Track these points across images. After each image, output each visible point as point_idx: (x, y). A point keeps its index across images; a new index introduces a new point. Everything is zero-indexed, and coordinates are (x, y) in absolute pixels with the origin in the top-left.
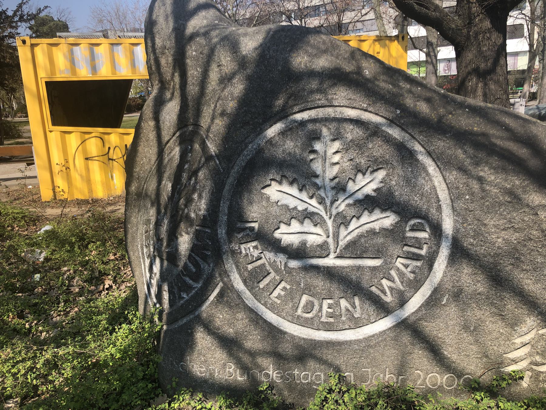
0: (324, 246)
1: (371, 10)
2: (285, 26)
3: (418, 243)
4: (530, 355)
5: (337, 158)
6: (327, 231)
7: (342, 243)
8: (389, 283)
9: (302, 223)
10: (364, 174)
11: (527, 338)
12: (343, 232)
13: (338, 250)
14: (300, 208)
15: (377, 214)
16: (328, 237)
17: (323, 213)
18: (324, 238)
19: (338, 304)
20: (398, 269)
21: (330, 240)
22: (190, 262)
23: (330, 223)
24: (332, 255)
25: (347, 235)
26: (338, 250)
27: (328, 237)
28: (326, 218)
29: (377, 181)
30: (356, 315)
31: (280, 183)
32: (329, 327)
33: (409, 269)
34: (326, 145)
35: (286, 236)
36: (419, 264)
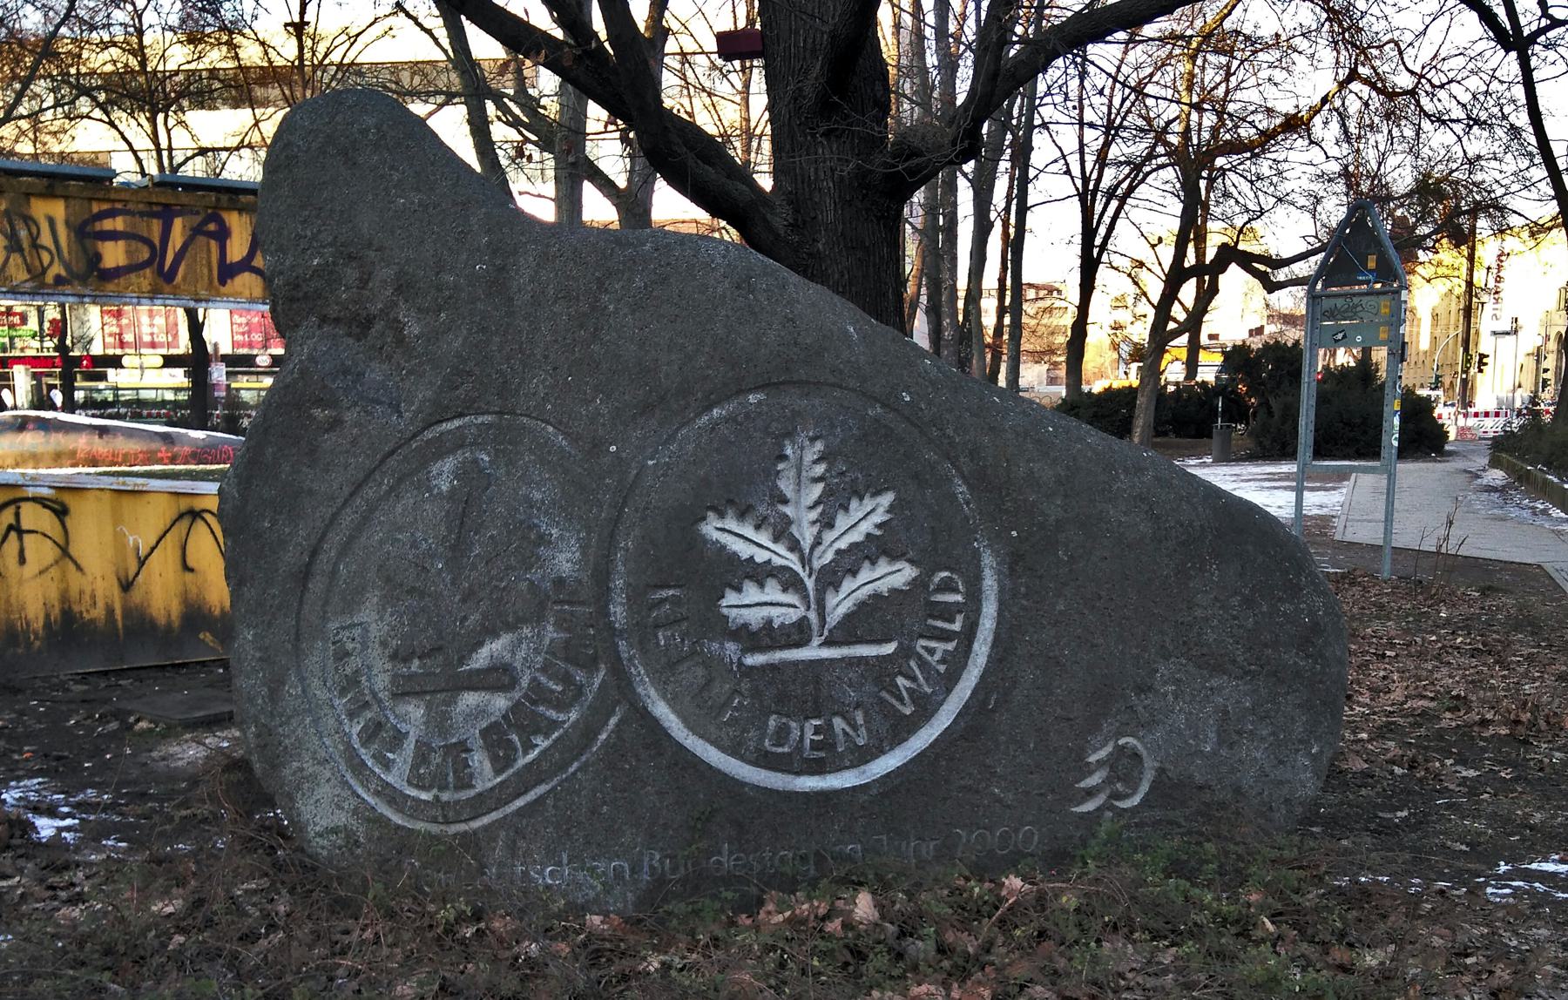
0: (802, 626)
1: (1148, 95)
2: (1189, 457)
3: (947, 613)
4: (1108, 781)
5: (820, 469)
6: (805, 597)
7: (834, 618)
8: (908, 684)
9: (762, 585)
10: (861, 499)
11: (1102, 754)
12: (831, 600)
13: (826, 633)
14: (758, 560)
15: (883, 567)
16: (809, 608)
17: (798, 568)
18: (801, 611)
19: (830, 725)
20: (920, 657)
21: (813, 616)
22: (516, 750)
23: (810, 584)
24: (816, 641)
25: (840, 604)
26: (826, 633)
27: (809, 608)
28: (803, 574)
29: (881, 510)
30: (861, 742)
31: (722, 515)
32: (818, 768)
33: (937, 657)
34: (802, 448)
35: (735, 610)
36: (950, 646)
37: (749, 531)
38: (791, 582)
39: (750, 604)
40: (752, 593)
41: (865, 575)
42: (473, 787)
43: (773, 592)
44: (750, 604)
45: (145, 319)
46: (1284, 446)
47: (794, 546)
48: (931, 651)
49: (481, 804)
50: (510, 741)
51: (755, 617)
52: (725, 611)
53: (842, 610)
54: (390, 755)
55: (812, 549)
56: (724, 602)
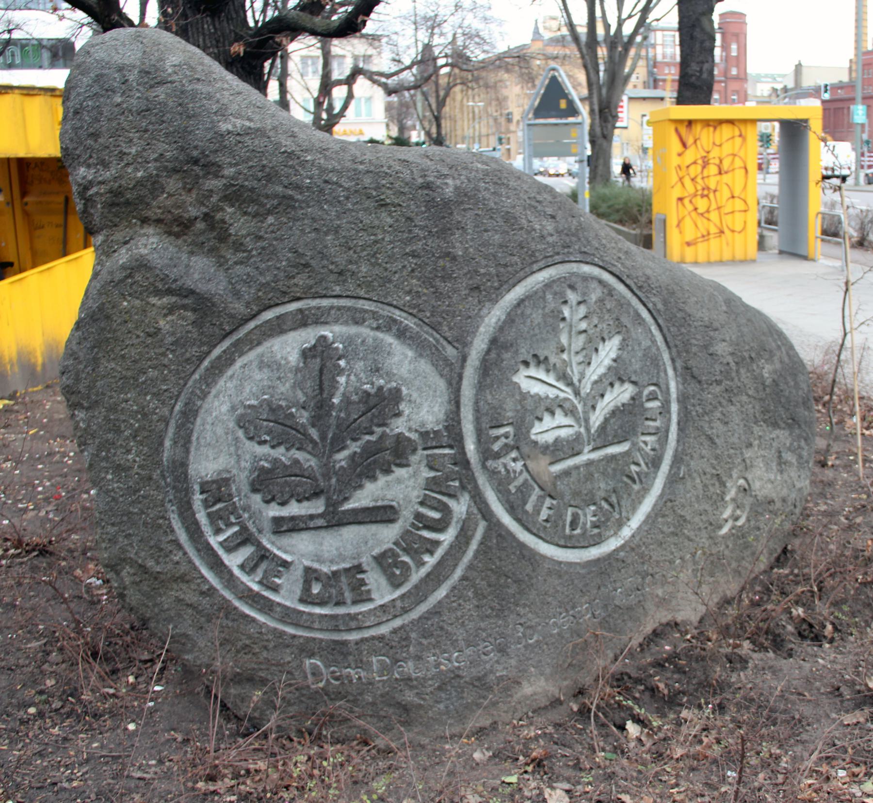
6: (577, 420)
14: (551, 396)
18: (576, 428)
21: (582, 430)
23: (580, 407)
24: (587, 449)
25: (596, 419)
37: (542, 375)
38: (570, 412)
39: (548, 429)
40: (548, 422)
41: (608, 397)
42: (371, 600)
43: (560, 419)
44: (548, 429)
45: (489, 397)
46: (688, 94)
47: (570, 384)
48: (645, 443)
49: (267, 607)
50: (403, 562)
51: (549, 438)
52: (533, 437)
53: (597, 424)
54: (277, 580)
55: (580, 381)
56: (534, 431)
